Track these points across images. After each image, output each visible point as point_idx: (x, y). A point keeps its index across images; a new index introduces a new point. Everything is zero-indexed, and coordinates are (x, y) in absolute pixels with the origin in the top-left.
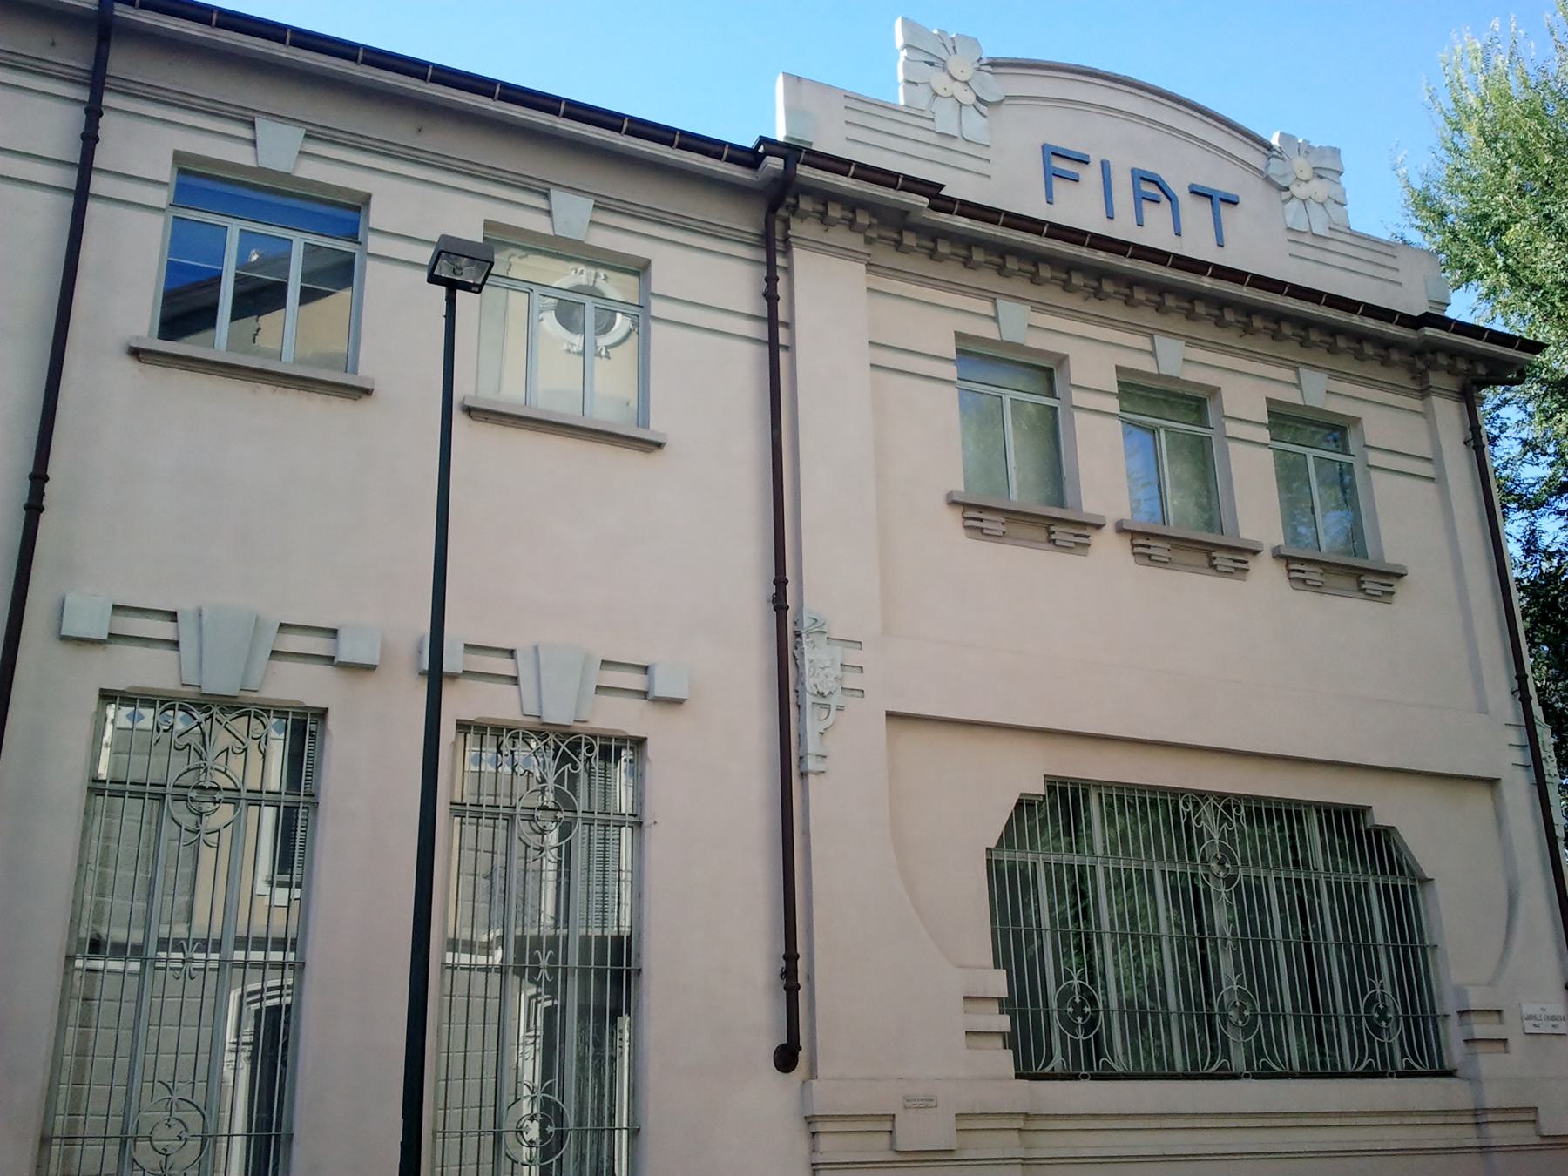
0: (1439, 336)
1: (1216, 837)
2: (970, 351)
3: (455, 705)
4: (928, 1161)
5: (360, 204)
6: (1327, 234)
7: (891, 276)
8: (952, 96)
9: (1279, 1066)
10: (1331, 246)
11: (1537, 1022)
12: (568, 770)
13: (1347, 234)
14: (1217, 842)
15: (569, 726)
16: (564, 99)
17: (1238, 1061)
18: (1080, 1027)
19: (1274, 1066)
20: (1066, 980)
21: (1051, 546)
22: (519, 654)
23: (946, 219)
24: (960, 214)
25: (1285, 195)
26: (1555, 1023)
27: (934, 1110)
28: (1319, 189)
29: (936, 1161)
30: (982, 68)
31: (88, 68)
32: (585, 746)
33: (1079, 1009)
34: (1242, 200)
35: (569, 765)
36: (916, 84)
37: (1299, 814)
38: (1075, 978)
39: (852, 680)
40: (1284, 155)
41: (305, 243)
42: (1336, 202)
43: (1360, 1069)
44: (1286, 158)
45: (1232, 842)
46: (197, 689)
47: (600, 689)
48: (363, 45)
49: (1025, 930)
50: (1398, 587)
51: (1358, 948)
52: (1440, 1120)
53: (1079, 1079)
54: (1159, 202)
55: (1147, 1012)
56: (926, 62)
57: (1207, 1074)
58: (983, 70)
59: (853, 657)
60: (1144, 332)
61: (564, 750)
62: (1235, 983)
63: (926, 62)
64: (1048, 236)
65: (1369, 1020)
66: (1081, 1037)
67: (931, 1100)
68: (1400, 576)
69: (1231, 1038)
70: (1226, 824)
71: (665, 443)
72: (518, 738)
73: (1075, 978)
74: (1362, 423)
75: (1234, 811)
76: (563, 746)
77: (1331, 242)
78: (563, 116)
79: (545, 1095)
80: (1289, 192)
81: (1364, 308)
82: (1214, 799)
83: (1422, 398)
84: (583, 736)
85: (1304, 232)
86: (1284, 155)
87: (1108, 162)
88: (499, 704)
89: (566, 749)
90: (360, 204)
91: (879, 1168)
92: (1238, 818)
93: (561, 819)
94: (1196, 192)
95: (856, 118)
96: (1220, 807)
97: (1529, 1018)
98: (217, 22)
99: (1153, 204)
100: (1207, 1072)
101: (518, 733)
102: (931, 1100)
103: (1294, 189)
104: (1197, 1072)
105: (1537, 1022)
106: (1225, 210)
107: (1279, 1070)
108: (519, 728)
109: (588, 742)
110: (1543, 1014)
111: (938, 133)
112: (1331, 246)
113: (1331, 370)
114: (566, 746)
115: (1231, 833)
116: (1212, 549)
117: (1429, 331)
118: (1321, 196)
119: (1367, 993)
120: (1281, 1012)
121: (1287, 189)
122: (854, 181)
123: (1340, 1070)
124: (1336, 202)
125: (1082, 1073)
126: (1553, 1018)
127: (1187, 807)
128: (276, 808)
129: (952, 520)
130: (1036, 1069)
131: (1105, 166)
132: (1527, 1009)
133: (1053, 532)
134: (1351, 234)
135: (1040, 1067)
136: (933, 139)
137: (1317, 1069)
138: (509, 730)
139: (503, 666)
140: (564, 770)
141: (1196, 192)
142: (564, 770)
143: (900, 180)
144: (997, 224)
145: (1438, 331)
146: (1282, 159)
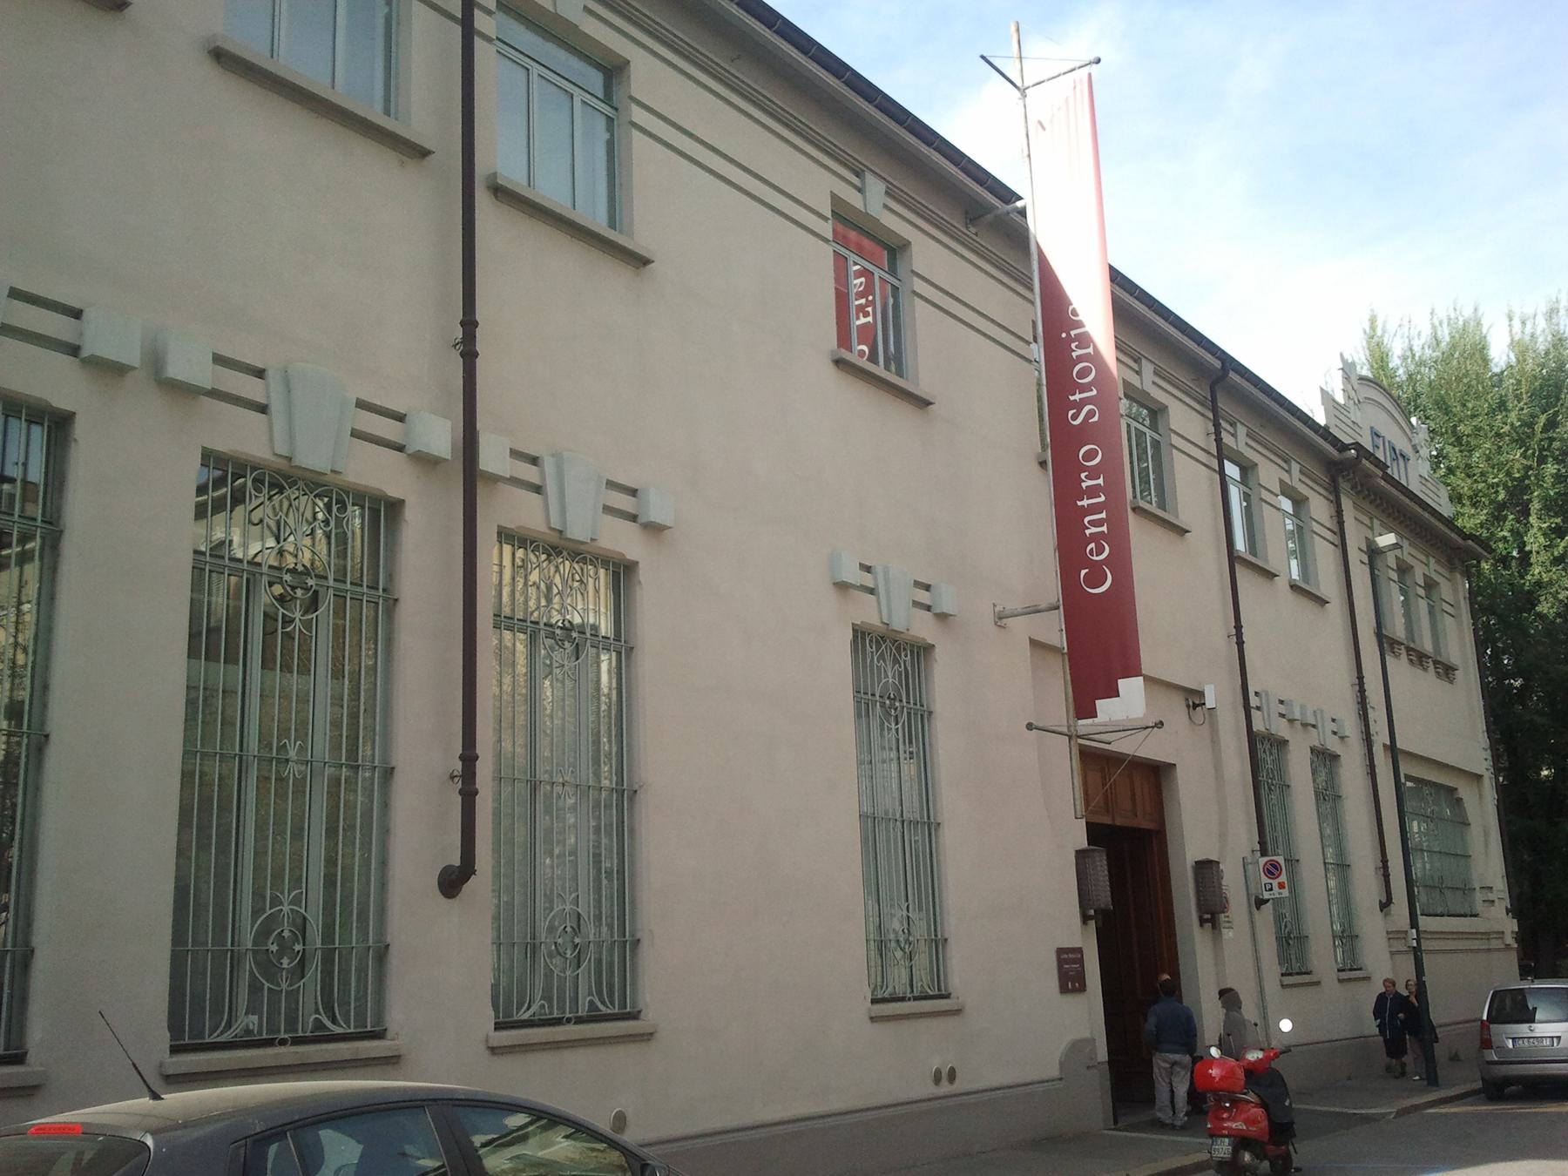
1: (890, 675)
2: (843, 215)
3: (500, 509)
15: (583, 543)
22: (270, 373)
23: (837, 84)
46: (886, 626)
47: (356, 434)
74: (1168, 412)
75: (903, 654)
79: (290, 907)
82: (568, 554)
83: (1451, 572)
84: (589, 557)
88: (526, 513)
92: (905, 662)
93: (312, 586)
95: (1338, 414)
96: (893, 649)
108: (589, 552)
109: (274, 481)
113: (891, 184)
136: (1351, 424)
138: (254, 469)
139: (250, 388)
143: (910, 119)
144: (839, 79)
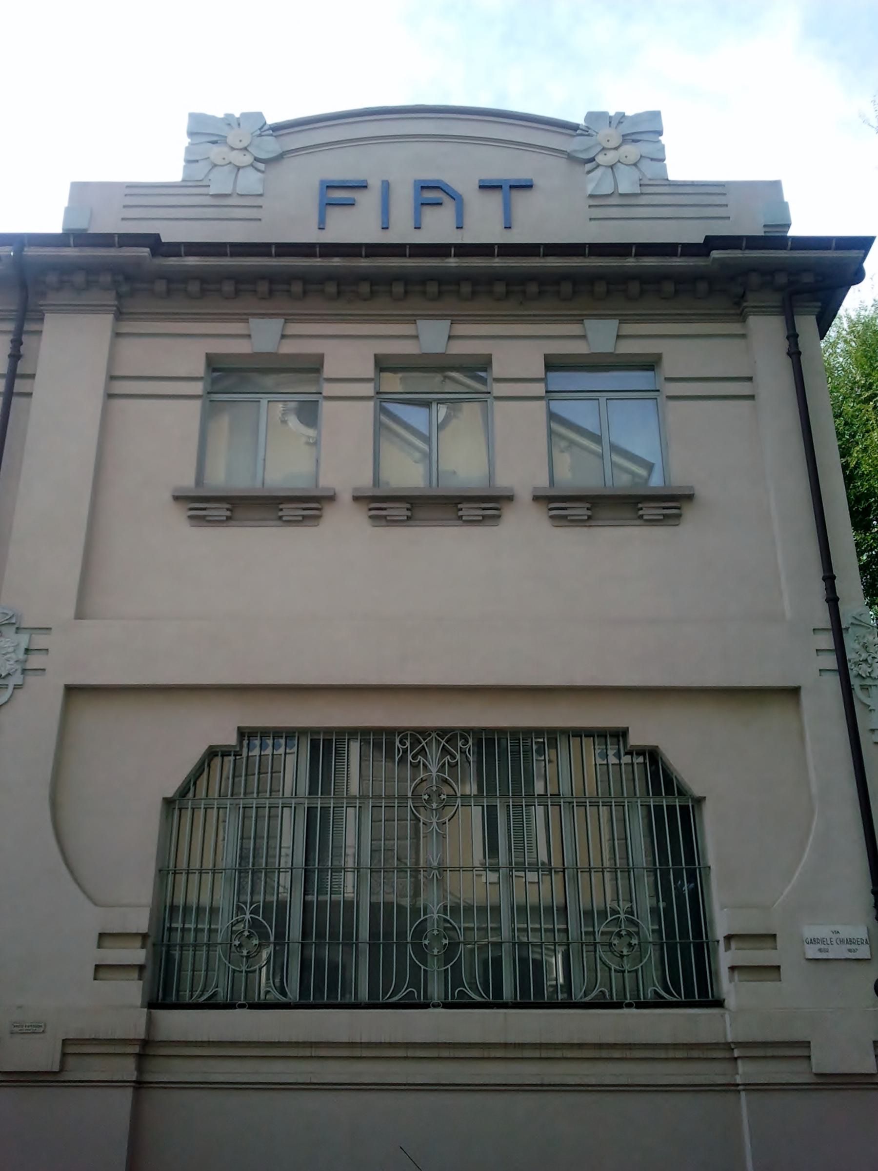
0: (730, 256)
4: (48, 1081)
6: (637, 190)
7: (142, 319)
8: (230, 163)
9: (672, 995)
10: (644, 200)
11: (822, 946)
12: (448, 761)
13: (666, 185)
14: (434, 774)
16: (496, 244)
17: (436, 991)
19: (473, 996)
21: (279, 523)
24: (187, 255)
25: (589, 166)
26: (853, 947)
27: (42, 1035)
28: (631, 151)
29: (29, 1082)
30: (263, 134)
31: (779, 304)
34: (536, 182)
35: (448, 757)
36: (197, 161)
37: (328, 742)
38: (248, 913)
39: (35, 661)
40: (590, 132)
42: (652, 159)
44: (594, 133)
48: (183, 243)
49: (673, 869)
50: (689, 512)
52: (679, 1054)
53: (236, 1008)
54: (441, 204)
55: (676, 943)
57: (386, 1004)
58: (263, 136)
59: (40, 641)
60: (655, 320)
62: (435, 912)
64: (411, 256)
67: (40, 1026)
68: (689, 498)
70: (448, 757)
72: (407, 739)
73: (248, 913)
75: (460, 744)
76: (443, 742)
77: (644, 197)
78: (454, 256)
80: (594, 163)
81: (682, 248)
82: (437, 734)
85: (230, 195)
86: (590, 132)
87: (480, 181)
90: (320, 358)
91: (240, 1089)
94: (485, 187)
97: (813, 941)
98: (185, 253)
99: (435, 208)
100: (387, 1001)
101: (407, 734)
102: (40, 1026)
103: (600, 159)
104: (377, 1001)
105: (822, 946)
107: (479, 999)
110: (834, 937)
111: (212, 195)
112: (644, 200)
114: (445, 742)
116: (457, 502)
117: (715, 254)
118: (632, 159)
120: (287, 941)
121: (592, 160)
122: (77, 249)
123: (642, 1000)
124: (652, 159)
125: (627, 1001)
126: (850, 941)
127: (404, 744)
128: (609, 807)
129: (178, 516)
130: (382, 999)
131: (386, 186)
132: (809, 932)
133: (461, 509)
134: (670, 185)
135: (386, 998)
137: (640, 999)
140: (445, 761)
141: (485, 187)
142: (445, 761)
145: (728, 251)
146: (588, 135)
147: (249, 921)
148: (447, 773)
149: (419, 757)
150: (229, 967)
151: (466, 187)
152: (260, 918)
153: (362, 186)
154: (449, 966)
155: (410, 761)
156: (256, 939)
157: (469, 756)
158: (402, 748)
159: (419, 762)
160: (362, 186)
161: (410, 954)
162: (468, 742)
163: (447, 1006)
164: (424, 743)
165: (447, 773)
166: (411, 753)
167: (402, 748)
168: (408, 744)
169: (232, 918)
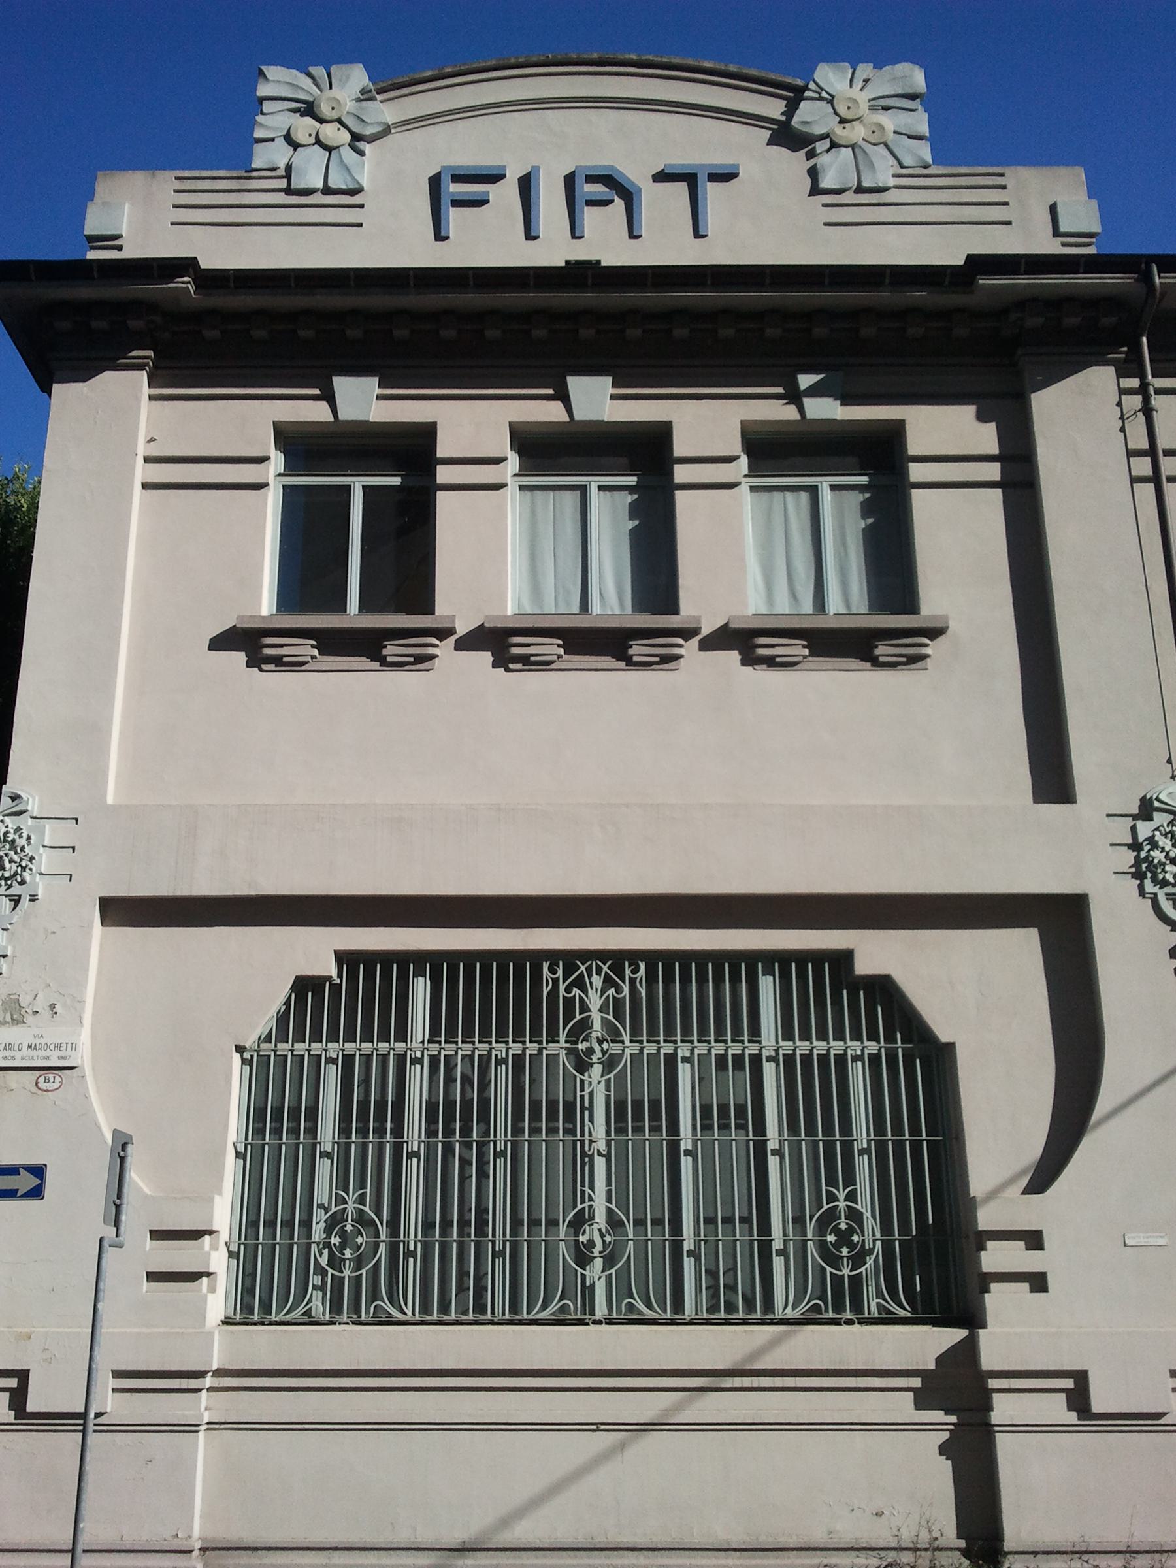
5: (428, 432)
18: (845, 1259)
20: (589, 1201)
32: (629, 967)
33: (844, 1238)
35: (613, 990)
38: (350, 1202)
41: (363, 486)
43: (544, 1315)
45: (618, 1015)
51: (899, 1146)
56: (289, 110)
61: (582, 972)
63: (289, 110)
65: (822, 1246)
66: (846, 1272)
69: (867, 1266)
70: (613, 990)
71: (948, 627)
75: (628, 972)
89: (609, 971)
90: (428, 432)
94: (662, 177)
106: (712, 192)
114: (608, 968)
115: (618, 1003)
119: (822, 1207)
140: (608, 996)
141: (662, 177)
147: (843, 1266)
148: (614, 1202)
149: (575, 989)
150: (862, 1207)
151: (637, 173)
152: (829, 1269)
153: (495, 177)
154: (578, 1017)
155: (563, 996)
156: (351, 1254)
157: (640, 988)
158: (551, 978)
159: (575, 996)
160: (495, 177)
161: (563, 1255)
162: (638, 972)
163: (610, 1322)
164: (583, 968)
165: (614, 1202)
166: (564, 982)
167: (551, 978)
168: (560, 973)
169: (866, 1269)
